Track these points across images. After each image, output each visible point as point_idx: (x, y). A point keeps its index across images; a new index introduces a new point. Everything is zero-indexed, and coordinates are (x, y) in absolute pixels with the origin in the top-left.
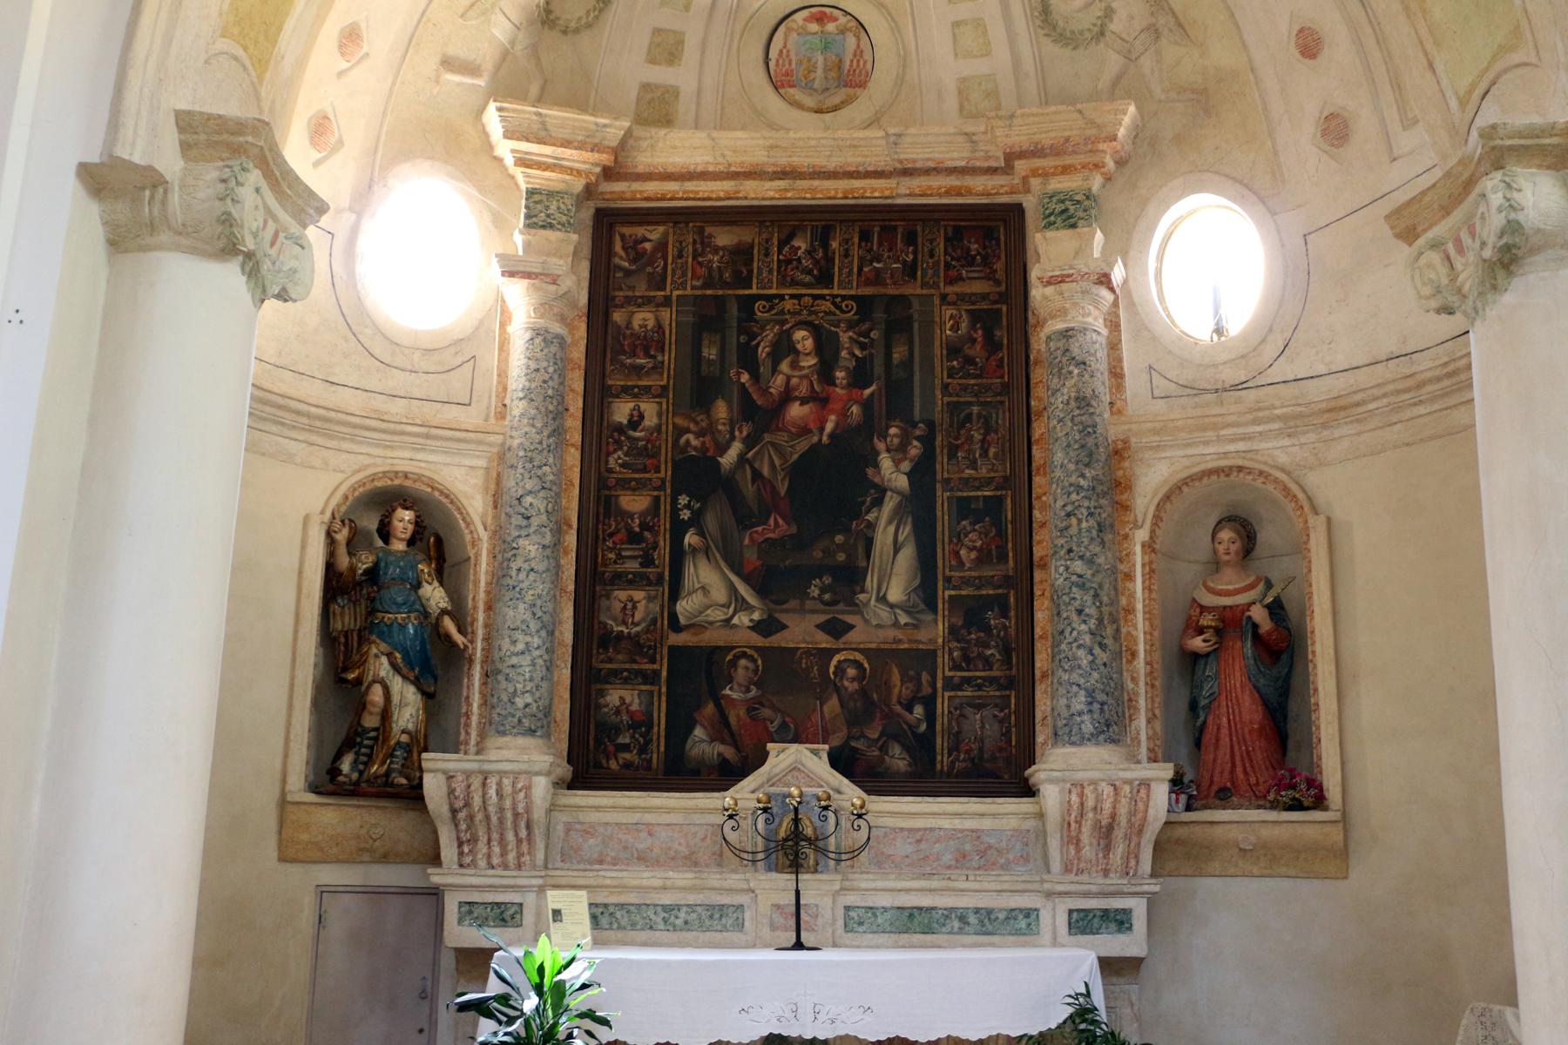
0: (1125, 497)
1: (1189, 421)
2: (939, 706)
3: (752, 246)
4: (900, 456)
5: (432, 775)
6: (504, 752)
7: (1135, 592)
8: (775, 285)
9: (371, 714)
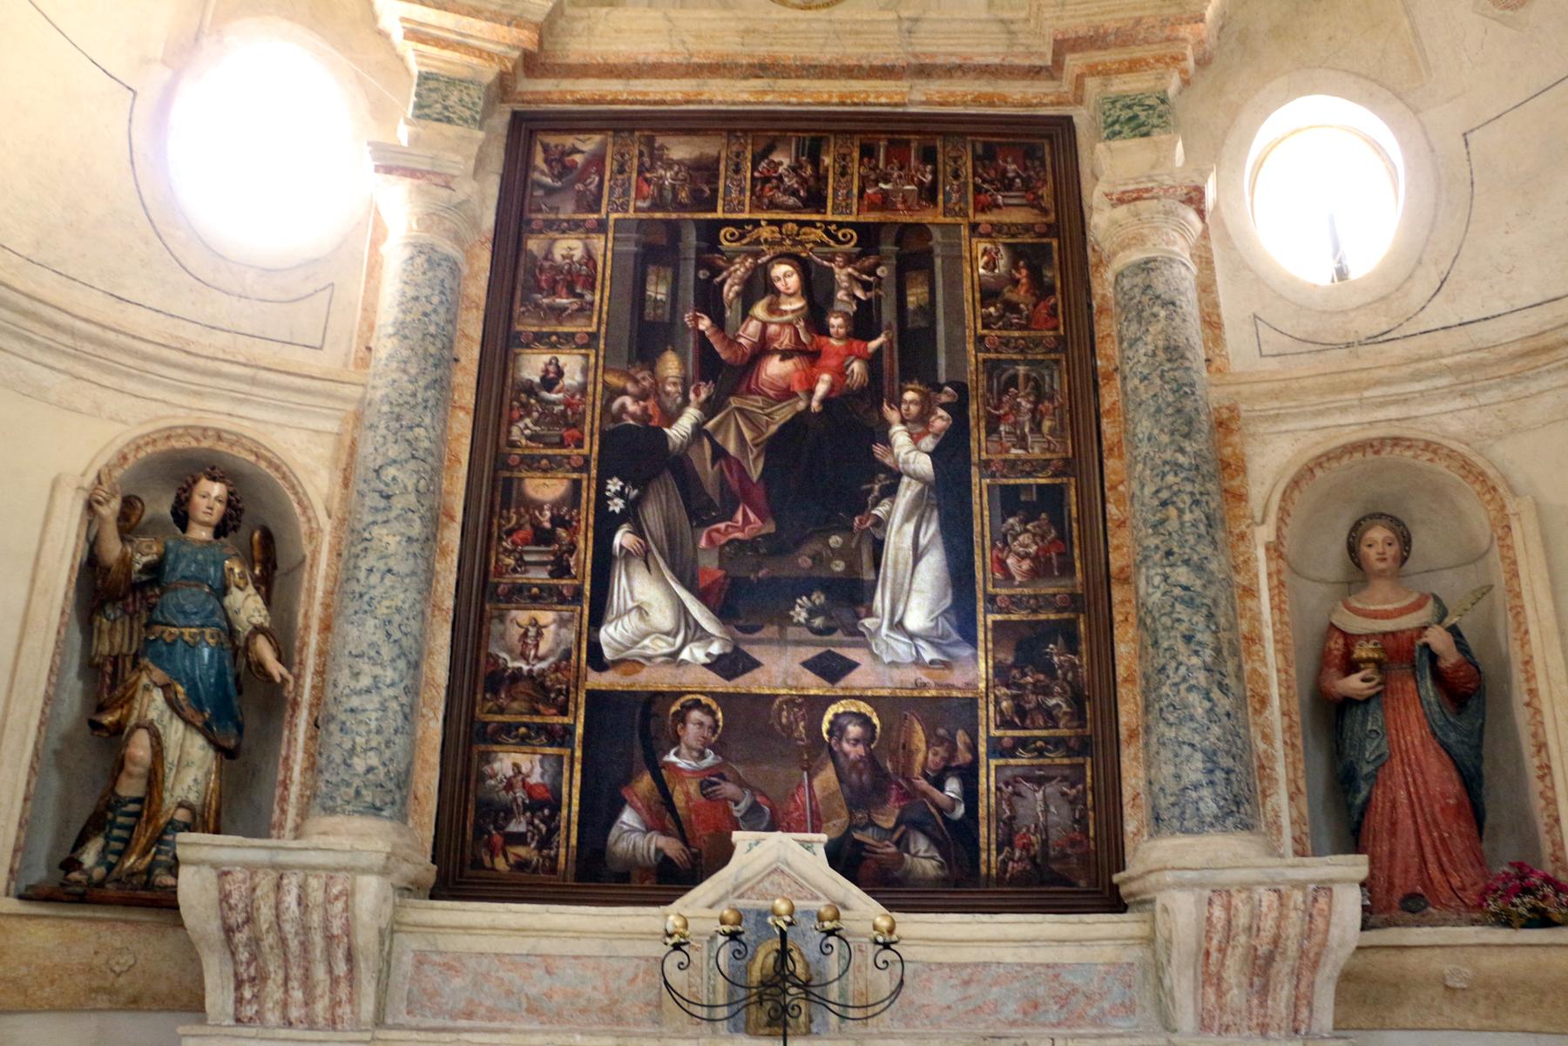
0: (1236, 483)
1: (1321, 380)
2: (983, 780)
3: (718, 160)
4: (920, 429)
5: (193, 869)
6: (331, 839)
7: (1260, 613)
8: (747, 208)
9: (130, 775)
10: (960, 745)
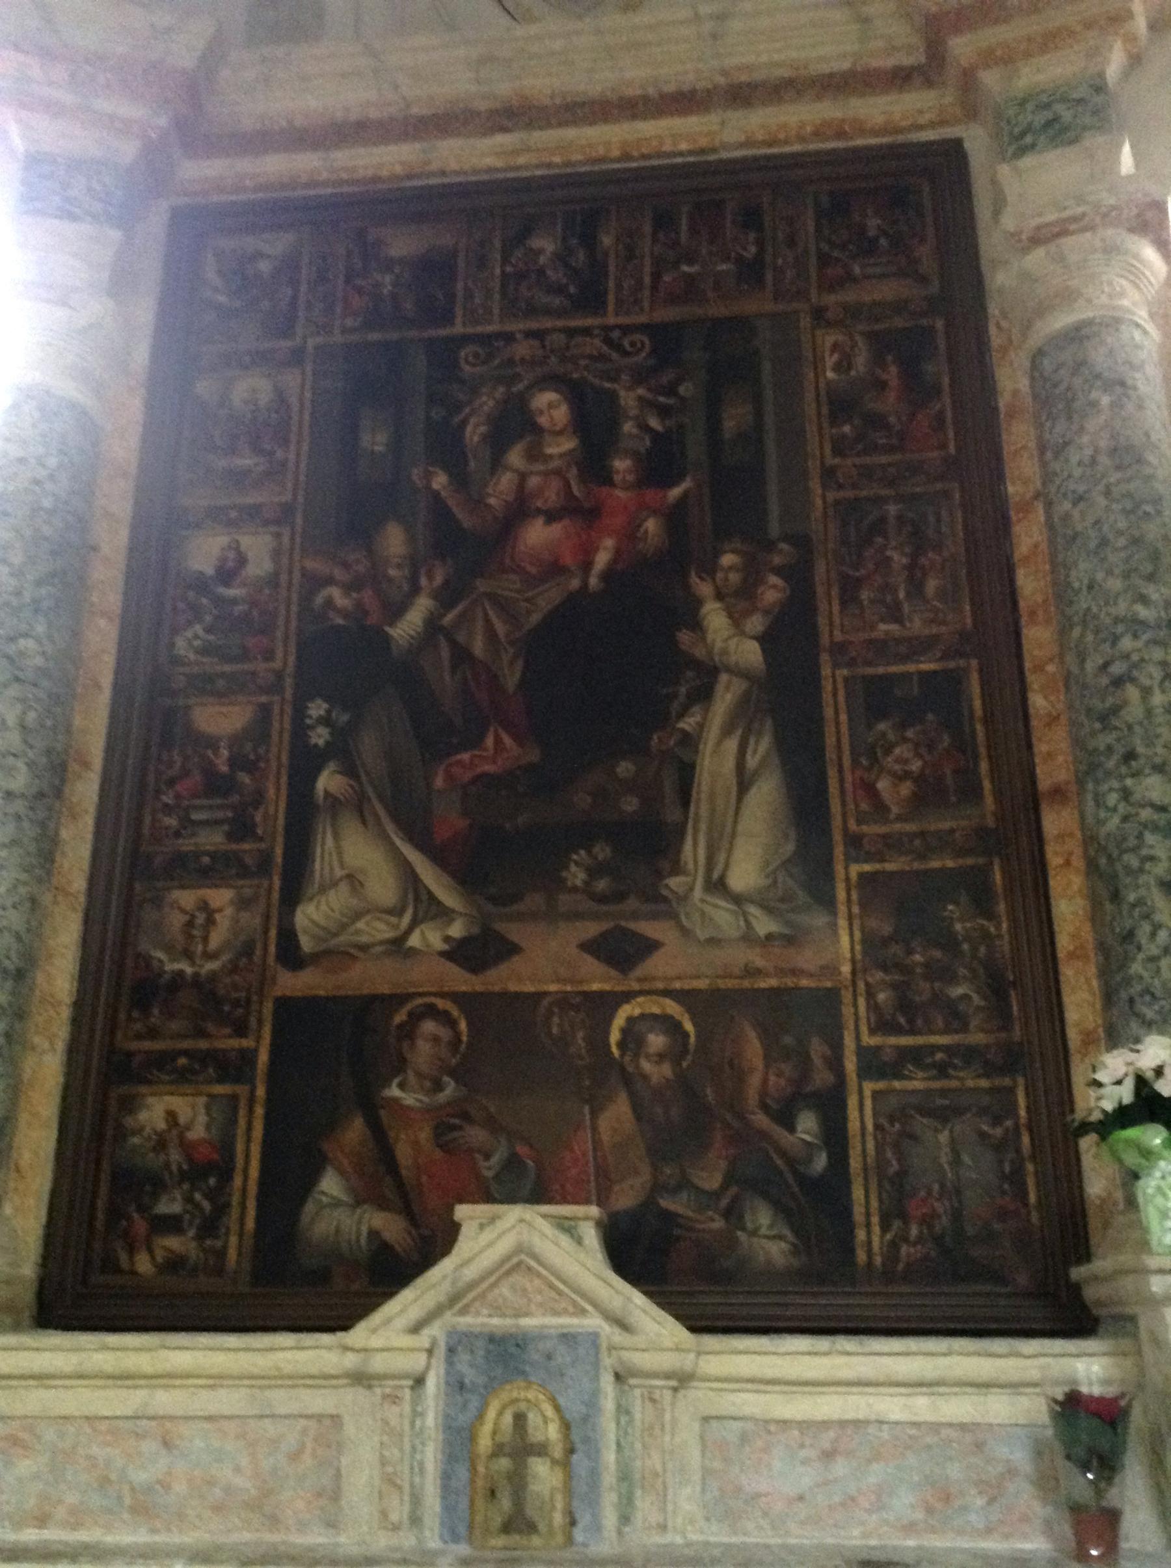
3: (454, 254)
8: (496, 318)
10: (817, 1061)
